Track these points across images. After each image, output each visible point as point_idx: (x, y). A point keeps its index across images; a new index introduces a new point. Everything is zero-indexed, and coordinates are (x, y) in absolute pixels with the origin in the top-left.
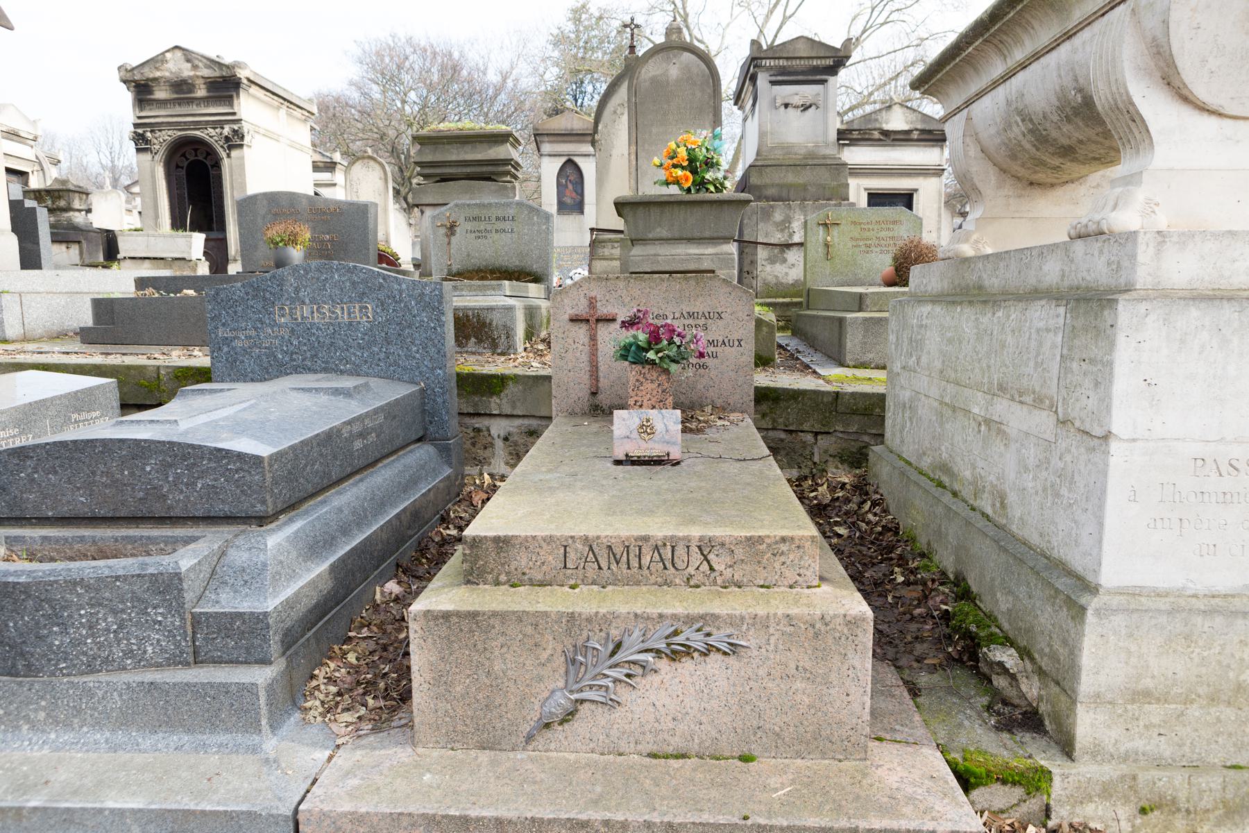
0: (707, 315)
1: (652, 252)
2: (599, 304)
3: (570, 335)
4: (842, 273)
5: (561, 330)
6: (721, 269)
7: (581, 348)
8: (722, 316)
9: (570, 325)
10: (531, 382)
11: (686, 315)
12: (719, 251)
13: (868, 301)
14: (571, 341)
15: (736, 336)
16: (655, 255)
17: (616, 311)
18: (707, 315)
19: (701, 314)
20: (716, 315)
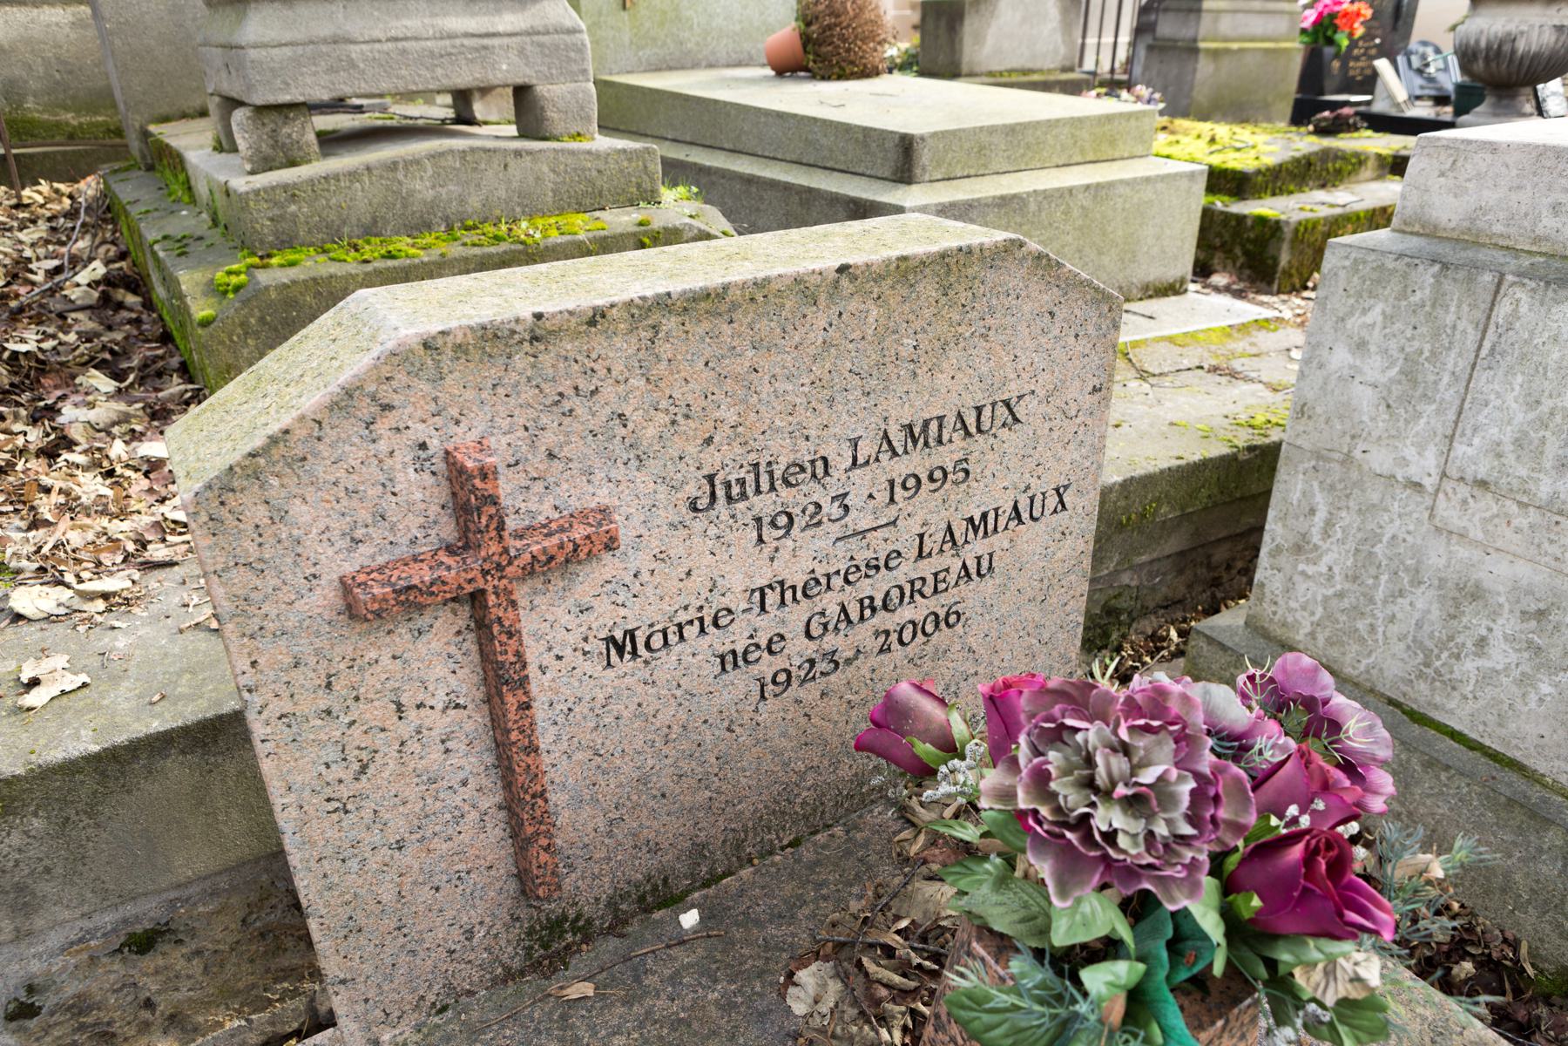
0: (971, 421)
1: (325, 30)
2: (506, 488)
3: (370, 682)
4: (654, 40)
5: (306, 678)
6: (550, 80)
7: (440, 723)
8: (1020, 412)
9: (351, 642)
10: (88, 784)
11: (898, 439)
12: (538, 23)
13: (924, 157)
14: (380, 711)
15: (1047, 484)
16: (335, 41)
17: (603, 495)
18: (971, 421)
19: (951, 420)
20: (1002, 411)
